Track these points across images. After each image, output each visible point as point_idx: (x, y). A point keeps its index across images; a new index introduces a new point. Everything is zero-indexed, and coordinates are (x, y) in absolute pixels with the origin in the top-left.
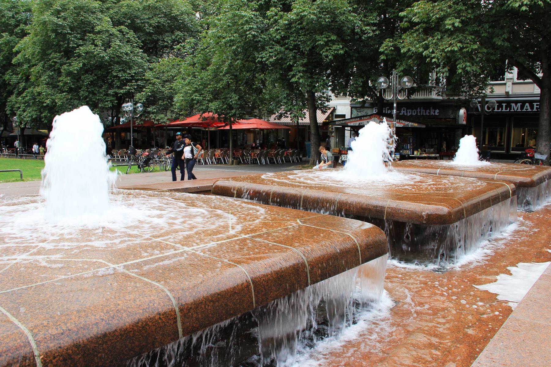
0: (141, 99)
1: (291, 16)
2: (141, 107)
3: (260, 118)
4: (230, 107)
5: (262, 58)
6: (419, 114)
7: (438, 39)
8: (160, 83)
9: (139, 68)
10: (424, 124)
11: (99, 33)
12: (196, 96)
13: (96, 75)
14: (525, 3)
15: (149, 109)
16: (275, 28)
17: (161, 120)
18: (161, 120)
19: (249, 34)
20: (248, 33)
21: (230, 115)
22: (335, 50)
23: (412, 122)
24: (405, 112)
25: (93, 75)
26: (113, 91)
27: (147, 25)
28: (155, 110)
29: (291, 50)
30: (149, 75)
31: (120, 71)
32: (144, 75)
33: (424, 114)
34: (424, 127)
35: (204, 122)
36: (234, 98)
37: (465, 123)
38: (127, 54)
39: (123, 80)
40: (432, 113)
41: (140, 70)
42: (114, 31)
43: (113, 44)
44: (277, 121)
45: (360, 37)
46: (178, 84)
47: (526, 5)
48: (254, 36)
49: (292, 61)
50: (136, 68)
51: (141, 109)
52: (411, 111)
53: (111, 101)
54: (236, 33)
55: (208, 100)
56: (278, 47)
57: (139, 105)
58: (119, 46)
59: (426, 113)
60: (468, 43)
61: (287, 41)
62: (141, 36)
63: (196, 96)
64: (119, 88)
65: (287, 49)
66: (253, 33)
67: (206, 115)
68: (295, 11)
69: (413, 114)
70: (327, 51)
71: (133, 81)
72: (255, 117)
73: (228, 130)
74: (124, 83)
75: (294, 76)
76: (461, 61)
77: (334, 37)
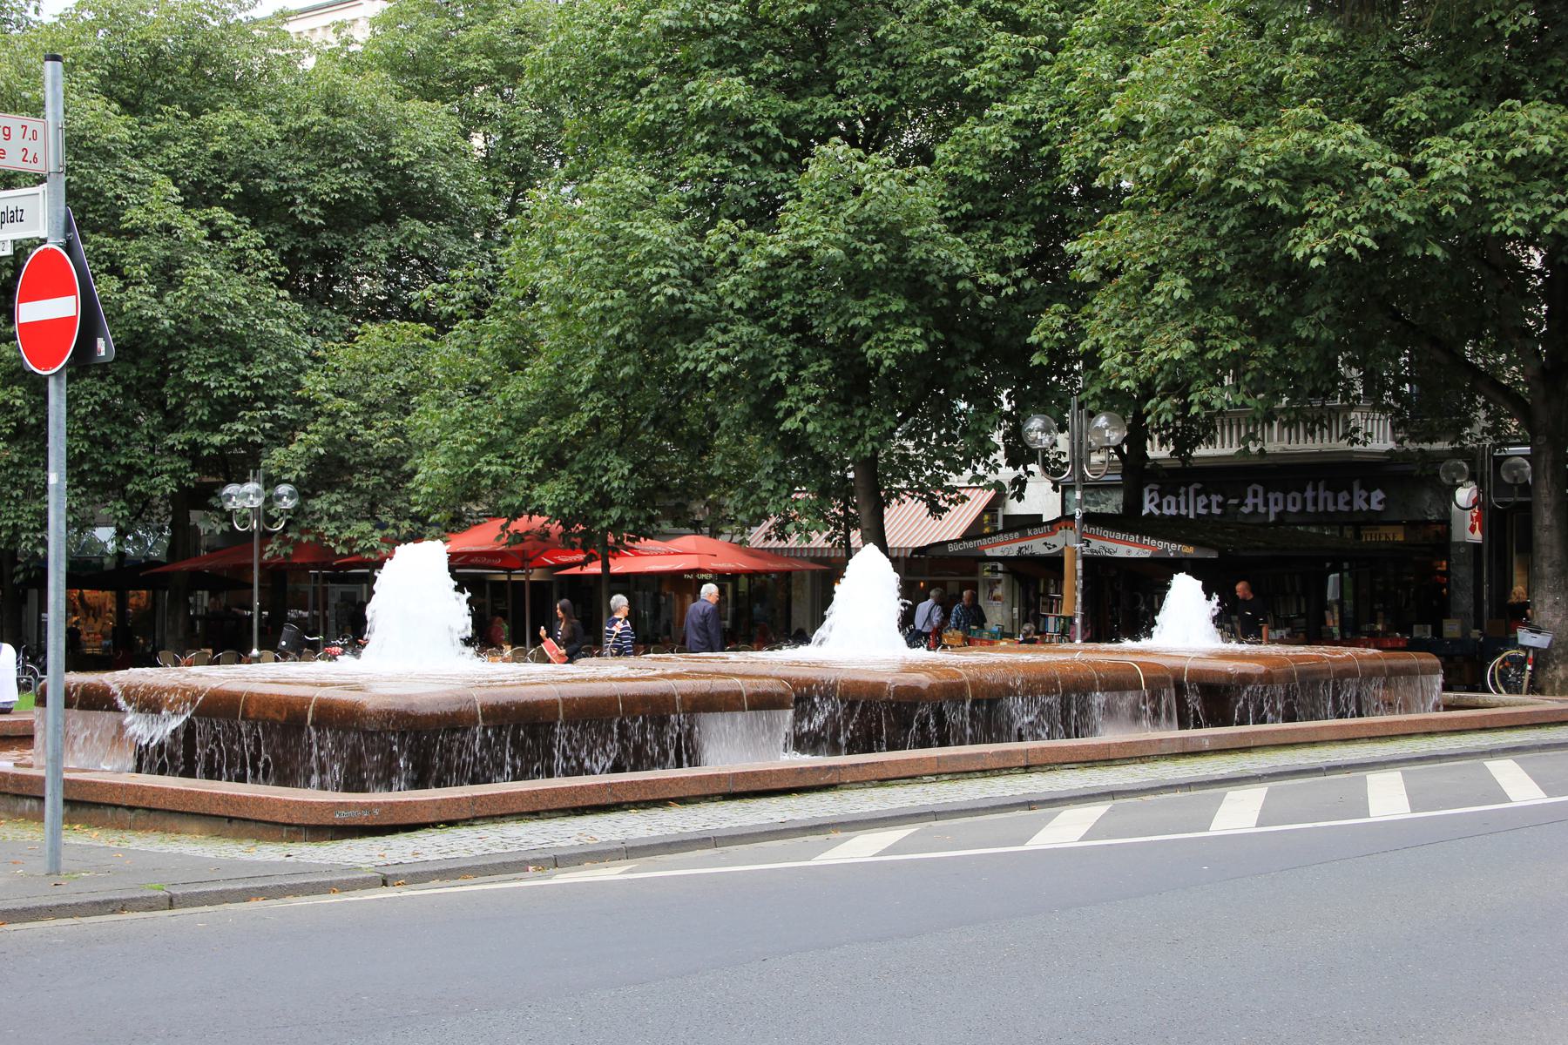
0: (290, 470)
1: (778, 245)
2: (291, 496)
3: (715, 534)
4: (604, 501)
5: (696, 361)
6: (1310, 508)
7: (1146, 326)
8: (355, 414)
9: (279, 359)
10: (1212, 547)
11: (133, 233)
12: (492, 465)
13: (118, 380)
14: (1317, 250)
15: (317, 504)
16: (732, 279)
17: (362, 543)
18: (362, 543)
19: (658, 293)
20: (654, 290)
21: (605, 524)
22: (901, 342)
23: (1177, 541)
24: (1260, 500)
25: (110, 379)
26: (184, 436)
27: (300, 200)
28: (339, 508)
29: (784, 333)
30: (313, 383)
31: (210, 368)
32: (298, 385)
33: (1331, 508)
34: (1214, 555)
35: (514, 548)
36: (617, 471)
37: (1477, 537)
38: (235, 307)
39: (219, 401)
40: (1359, 504)
41: (283, 365)
42: (189, 225)
43: (189, 274)
44: (774, 543)
45: (975, 303)
46: (426, 419)
47: (1321, 253)
48: (672, 299)
49: (785, 368)
50: (271, 357)
51: (289, 504)
52: (1280, 495)
53: (173, 473)
54: (617, 287)
55: (529, 477)
56: (743, 330)
57: (283, 489)
58: (208, 280)
59: (1336, 503)
60: (1216, 337)
61: (774, 303)
62: (277, 235)
63: (492, 465)
64: (202, 426)
65: (773, 328)
66: (669, 291)
67: (521, 524)
68: (785, 233)
69: (1291, 509)
70: (879, 343)
71: (261, 404)
72: (696, 527)
73: (596, 576)
74: (227, 410)
75: (790, 413)
76: (1202, 383)
77: (898, 305)
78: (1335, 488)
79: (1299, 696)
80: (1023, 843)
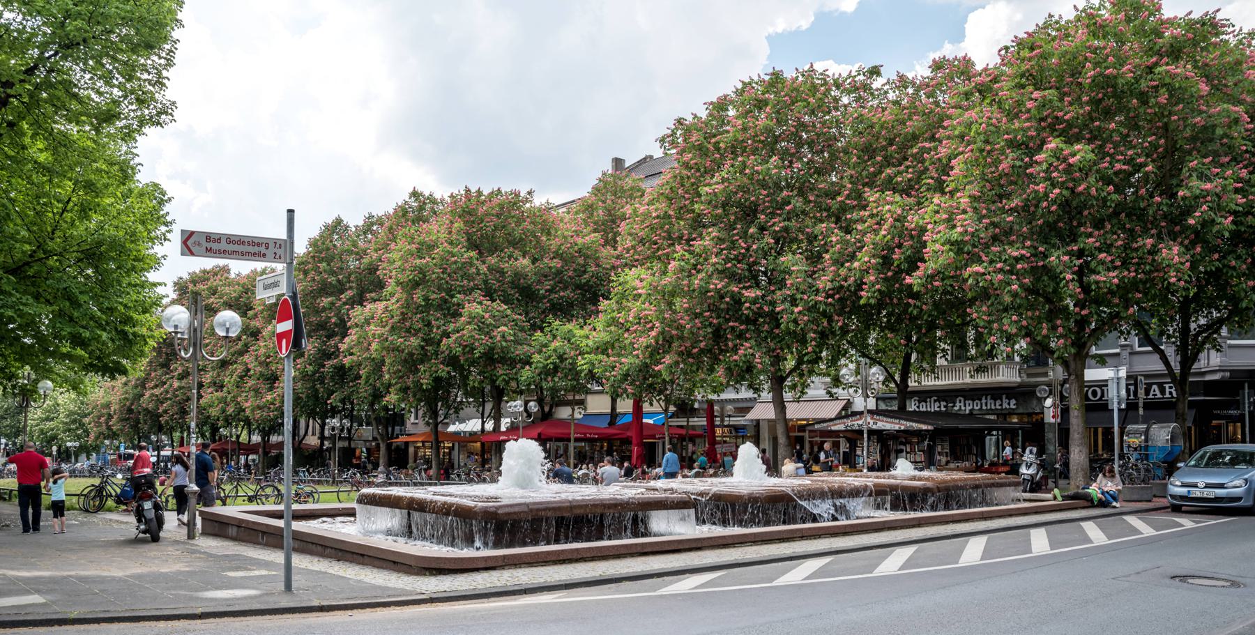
34: (930, 428)
40: (1005, 405)
78: (994, 399)
79: (948, 496)
80: (771, 580)
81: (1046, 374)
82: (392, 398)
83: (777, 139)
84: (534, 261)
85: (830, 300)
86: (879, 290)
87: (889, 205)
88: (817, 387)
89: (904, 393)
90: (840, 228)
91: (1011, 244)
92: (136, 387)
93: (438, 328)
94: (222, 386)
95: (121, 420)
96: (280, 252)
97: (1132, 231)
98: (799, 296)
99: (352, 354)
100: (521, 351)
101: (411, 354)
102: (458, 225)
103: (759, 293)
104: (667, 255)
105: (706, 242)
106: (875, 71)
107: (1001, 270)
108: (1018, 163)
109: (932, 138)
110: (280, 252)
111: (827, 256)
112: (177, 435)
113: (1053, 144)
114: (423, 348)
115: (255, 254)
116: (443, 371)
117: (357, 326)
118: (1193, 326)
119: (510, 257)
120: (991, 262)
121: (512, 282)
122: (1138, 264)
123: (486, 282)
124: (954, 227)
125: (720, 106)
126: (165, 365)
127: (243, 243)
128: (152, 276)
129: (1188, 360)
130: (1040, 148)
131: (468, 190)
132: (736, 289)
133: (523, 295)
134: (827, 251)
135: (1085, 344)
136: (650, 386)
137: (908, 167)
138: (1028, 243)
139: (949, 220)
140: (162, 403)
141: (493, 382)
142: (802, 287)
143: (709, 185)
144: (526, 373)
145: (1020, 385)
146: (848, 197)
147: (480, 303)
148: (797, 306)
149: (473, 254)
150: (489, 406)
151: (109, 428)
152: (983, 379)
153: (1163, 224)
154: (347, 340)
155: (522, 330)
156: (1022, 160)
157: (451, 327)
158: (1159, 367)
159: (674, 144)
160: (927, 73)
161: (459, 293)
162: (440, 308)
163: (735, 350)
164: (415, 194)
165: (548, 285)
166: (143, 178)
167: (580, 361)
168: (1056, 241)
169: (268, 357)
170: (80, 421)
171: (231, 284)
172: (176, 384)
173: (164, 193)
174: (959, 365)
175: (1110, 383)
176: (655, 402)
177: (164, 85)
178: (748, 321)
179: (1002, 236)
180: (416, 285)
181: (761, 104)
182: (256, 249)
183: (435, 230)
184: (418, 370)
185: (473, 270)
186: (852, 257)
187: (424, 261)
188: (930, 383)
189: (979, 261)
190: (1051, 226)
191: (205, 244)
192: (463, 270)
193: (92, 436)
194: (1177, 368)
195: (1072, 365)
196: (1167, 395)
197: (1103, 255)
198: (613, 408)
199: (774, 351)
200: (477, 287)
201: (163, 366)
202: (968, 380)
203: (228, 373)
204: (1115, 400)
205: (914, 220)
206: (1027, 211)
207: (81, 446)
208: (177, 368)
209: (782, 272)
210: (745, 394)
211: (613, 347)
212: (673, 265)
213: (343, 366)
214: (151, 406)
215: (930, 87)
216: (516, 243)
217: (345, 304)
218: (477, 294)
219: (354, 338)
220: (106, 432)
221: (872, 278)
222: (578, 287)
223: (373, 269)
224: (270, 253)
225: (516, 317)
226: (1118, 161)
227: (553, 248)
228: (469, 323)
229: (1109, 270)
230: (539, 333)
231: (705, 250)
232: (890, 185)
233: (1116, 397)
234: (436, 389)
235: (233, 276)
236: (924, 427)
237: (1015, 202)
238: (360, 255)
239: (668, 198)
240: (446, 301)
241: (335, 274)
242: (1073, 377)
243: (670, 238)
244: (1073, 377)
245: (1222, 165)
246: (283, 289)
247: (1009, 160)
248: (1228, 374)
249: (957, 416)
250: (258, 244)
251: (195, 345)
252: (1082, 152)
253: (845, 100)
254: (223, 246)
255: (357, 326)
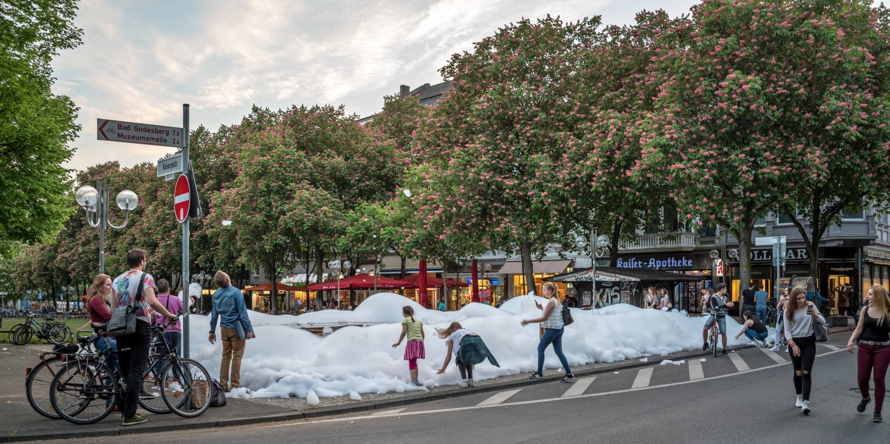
34: (638, 280)
40: (684, 264)
81: (713, 242)
82: (243, 259)
83: (527, 70)
84: (347, 159)
85: (567, 188)
86: (605, 182)
87: (613, 119)
88: (552, 253)
89: (614, 254)
90: (574, 135)
91: (703, 146)
92: (50, 251)
93: (277, 208)
94: (115, 251)
95: (40, 276)
96: (178, 138)
97: (787, 138)
98: (545, 184)
99: (212, 227)
100: (337, 224)
101: (257, 227)
102: (290, 131)
103: (516, 182)
104: (448, 155)
105: (478, 143)
106: (596, 20)
107: (696, 166)
108: (709, 88)
109: (641, 71)
110: (178, 138)
111: (565, 156)
112: (81, 286)
113: (734, 74)
114: (265, 222)
115: (157, 140)
116: (281, 239)
117: (216, 206)
118: (822, 208)
119: (329, 156)
120: (689, 160)
121: (331, 174)
122: (792, 162)
123: (311, 174)
124: (662, 134)
125: (484, 46)
126: (72, 235)
127: (148, 131)
128: (64, 165)
129: (817, 234)
130: (723, 78)
131: (294, 107)
132: (500, 179)
133: (340, 184)
134: (565, 152)
135: (751, 221)
136: (433, 249)
137: (624, 92)
138: (715, 146)
139: (659, 129)
140: (71, 263)
141: (317, 247)
142: (548, 177)
143: (478, 103)
144: (343, 241)
145: (696, 250)
146: (578, 112)
147: (307, 189)
148: (543, 191)
149: (302, 153)
150: (312, 265)
151: (31, 281)
152: (669, 245)
153: (810, 134)
154: (209, 216)
155: (339, 209)
156: (711, 86)
157: (286, 207)
158: (799, 237)
159: (451, 73)
160: (635, 23)
161: (292, 182)
162: (278, 192)
163: (498, 223)
164: (255, 109)
165: (357, 176)
166: (56, 90)
167: (382, 232)
168: (734, 144)
169: (150, 229)
170: (8, 277)
171: (121, 175)
172: (80, 250)
173: (72, 104)
174: (652, 235)
175: (774, 248)
176: (437, 262)
177: (73, 13)
178: (508, 202)
179: (696, 141)
180: (260, 176)
181: (514, 44)
182: (158, 136)
183: (272, 136)
184: (263, 239)
185: (302, 166)
186: (584, 156)
187: (265, 158)
188: (631, 248)
189: (681, 160)
190: (732, 135)
191: (117, 131)
192: (294, 165)
193: (18, 288)
194: (810, 237)
195: (742, 235)
196: (799, 257)
197: (768, 153)
198: (403, 266)
199: (526, 224)
200: (304, 178)
201: (70, 236)
202: (659, 246)
203: (119, 241)
204: (778, 260)
205: (630, 131)
206: (712, 125)
207: (9, 295)
208: (81, 237)
209: (531, 166)
210: (501, 255)
211: (406, 220)
212: (452, 162)
213: (206, 236)
214: (62, 266)
215: (638, 33)
216: (333, 146)
217: (208, 190)
218: (305, 183)
219: (214, 215)
220: (28, 285)
221: (600, 172)
222: (379, 178)
223: (226, 164)
224: (169, 139)
225: (333, 200)
226: (780, 86)
227: (361, 149)
228: (299, 204)
229: (772, 165)
230: (352, 211)
231: (476, 151)
232: (609, 105)
233: (780, 258)
234: (275, 251)
235: (121, 170)
236: (634, 279)
237: (706, 117)
238: (219, 153)
239: (448, 113)
240: (282, 188)
241: (205, 162)
242: (742, 243)
243: (450, 142)
244: (742, 243)
245: (853, 91)
246: (181, 168)
247: (702, 86)
248: (842, 242)
249: (652, 270)
250: (160, 132)
251: (102, 216)
252: (753, 82)
253: (576, 42)
254: (132, 132)
255: (216, 206)
